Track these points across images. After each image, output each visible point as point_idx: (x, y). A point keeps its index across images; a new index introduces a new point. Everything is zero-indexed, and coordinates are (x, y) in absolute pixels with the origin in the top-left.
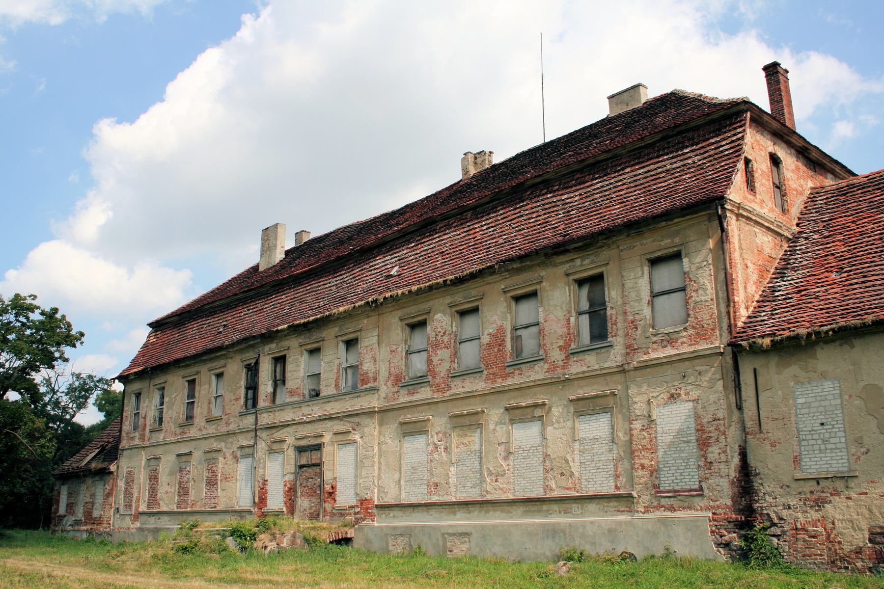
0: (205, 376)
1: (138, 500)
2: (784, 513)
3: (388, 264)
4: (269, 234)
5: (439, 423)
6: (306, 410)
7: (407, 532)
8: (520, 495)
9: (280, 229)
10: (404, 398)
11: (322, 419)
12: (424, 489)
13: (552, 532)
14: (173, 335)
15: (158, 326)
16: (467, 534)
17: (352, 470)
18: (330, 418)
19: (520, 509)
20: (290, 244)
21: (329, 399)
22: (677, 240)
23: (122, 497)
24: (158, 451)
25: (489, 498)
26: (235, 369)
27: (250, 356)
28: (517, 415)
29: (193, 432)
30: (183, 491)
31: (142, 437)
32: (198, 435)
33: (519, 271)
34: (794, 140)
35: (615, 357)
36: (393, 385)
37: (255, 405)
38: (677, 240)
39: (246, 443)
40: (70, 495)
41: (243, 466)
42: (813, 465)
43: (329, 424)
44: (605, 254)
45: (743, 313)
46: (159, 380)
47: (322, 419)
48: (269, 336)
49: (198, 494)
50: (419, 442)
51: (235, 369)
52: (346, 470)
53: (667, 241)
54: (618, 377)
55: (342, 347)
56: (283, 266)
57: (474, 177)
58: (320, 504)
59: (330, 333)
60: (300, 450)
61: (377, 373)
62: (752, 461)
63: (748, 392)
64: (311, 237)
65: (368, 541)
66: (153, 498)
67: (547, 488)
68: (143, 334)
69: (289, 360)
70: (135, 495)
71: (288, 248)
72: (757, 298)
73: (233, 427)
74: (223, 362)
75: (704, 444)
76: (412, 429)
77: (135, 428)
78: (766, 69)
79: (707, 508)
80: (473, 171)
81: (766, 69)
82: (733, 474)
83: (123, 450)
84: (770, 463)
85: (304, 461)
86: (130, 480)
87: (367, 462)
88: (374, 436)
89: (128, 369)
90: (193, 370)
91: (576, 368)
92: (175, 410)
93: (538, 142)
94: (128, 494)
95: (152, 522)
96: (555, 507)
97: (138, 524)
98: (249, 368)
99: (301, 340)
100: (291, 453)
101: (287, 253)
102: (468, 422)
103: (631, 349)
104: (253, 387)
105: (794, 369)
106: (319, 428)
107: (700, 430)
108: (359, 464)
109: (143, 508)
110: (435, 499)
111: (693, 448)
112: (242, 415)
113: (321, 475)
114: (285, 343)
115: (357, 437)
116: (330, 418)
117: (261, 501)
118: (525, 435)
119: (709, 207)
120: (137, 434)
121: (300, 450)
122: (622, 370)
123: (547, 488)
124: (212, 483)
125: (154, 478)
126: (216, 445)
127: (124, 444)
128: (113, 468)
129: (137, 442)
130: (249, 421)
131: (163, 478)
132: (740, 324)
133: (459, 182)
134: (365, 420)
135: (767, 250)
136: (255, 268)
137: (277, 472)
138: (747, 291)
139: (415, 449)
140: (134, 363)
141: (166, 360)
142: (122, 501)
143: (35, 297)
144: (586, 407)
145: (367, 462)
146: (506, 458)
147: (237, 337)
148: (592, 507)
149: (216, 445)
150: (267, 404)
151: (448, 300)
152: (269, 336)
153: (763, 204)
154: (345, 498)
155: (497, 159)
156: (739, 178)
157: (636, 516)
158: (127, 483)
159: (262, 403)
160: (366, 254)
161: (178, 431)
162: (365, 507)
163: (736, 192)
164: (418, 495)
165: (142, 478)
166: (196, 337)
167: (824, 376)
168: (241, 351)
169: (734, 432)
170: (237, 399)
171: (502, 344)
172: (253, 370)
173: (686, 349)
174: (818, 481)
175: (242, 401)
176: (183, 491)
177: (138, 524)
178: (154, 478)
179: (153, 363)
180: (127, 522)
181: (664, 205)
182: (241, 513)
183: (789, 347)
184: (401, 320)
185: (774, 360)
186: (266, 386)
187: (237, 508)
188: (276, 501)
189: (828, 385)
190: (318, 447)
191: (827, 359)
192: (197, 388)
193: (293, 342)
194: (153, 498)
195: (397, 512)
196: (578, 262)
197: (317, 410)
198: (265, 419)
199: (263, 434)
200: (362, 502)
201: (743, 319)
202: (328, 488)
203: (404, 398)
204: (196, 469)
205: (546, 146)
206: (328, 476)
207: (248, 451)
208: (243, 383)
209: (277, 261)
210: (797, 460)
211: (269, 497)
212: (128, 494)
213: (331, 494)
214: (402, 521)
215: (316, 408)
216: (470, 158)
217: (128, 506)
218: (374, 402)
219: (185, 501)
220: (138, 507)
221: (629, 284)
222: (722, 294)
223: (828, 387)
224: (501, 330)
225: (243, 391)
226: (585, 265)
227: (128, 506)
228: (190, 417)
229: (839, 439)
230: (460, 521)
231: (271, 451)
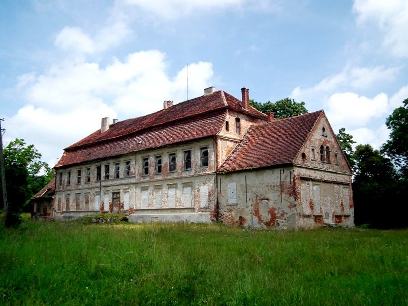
0: (84, 169)
1: (63, 208)
2: (224, 213)
3: (138, 139)
4: (104, 120)
5: (151, 188)
6: (115, 182)
7: (142, 217)
8: (170, 207)
9: (107, 119)
10: (142, 180)
11: (119, 185)
12: (147, 205)
13: (177, 217)
14: (73, 154)
15: (67, 150)
16: (157, 217)
17: (128, 200)
18: (122, 185)
19: (169, 211)
20: (111, 123)
21: (122, 179)
22: (207, 144)
23: (57, 207)
24: (69, 192)
25: (163, 208)
26: (93, 168)
27: (98, 164)
28: (170, 186)
29: (80, 187)
30: (78, 205)
31: (63, 188)
32: (82, 187)
33: (171, 147)
34: (245, 113)
35: (192, 173)
36: (139, 176)
37: (100, 179)
38: (207, 144)
39: (97, 191)
40: (38, 206)
41: (97, 197)
42: (230, 202)
43: (122, 186)
44: (192, 145)
45: (220, 164)
46: (68, 170)
47: (119, 185)
48: (104, 159)
49: (83, 206)
50: (146, 193)
51: (93, 168)
52: (127, 200)
53: (204, 144)
54: (193, 178)
55: (125, 163)
56: (109, 132)
57: (167, 109)
58: (120, 209)
59: (122, 159)
60: (114, 193)
61: (135, 172)
62: (219, 201)
63: (219, 184)
64: (119, 121)
65: (132, 219)
66: (68, 207)
67: (176, 206)
68: (61, 154)
69: (110, 167)
70: (62, 206)
71: (110, 124)
72: (225, 159)
73: (93, 186)
74: (90, 165)
75: (210, 196)
76: (144, 189)
77: (61, 184)
78: (242, 89)
79: (209, 212)
80: (167, 107)
81: (242, 89)
82: (215, 203)
83: (57, 192)
84: (223, 202)
85: (115, 197)
86: (59, 201)
87: (132, 198)
88: (135, 191)
89: (57, 165)
90: (80, 167)
91: (184, 175)
92: (74, 179)
93: (186, 100)
94: (59, 206)
95: (68, 215)
96: (178, 211)
97: (63, 215)
98: (98, 168)
99: (113, 161)
100: (111, 194)
101: (111, 126)
102: (158, 188)
103: (196, 171)
104: (99, 174)
105: (228, 179)
106: (119, 187)
107: (209, 193)
108: (130, 198)
109: (64, 210)
110: (150, 208)
111: (207, 197)
112: (96, 182)
113: (120, 201)
114: (109, 161)
115: (129, 190)
116: (122, 185)
117: (103, 208)
118: (172, 192)
119: (214, 138)
120: (61, 187)
121: (114, 193)
122: (193, 176)
123: (176, 206)
124: (87, 203)
125: (68, 201)
126: (88, 191)
127: (57, 190)
128: (53, 197)
129: (61, 189)
130: (99, 184)
131: (71, 201)
132: (219, 167)
133: (162, 110)
134: (132, 186)
135: (231, 146)
136: (99, 132)
137: (107, 200)
138: (222, 157)
139: (145, 195)
140: (59, 163)
141: (71, 163)
142: (57, 208)
143: (23, 140)
144: (185, 185)
145: (132, 198)
146: (167, 198)
147: (94, 158)
148: (186, 211)
149: (88, 191)
150: (104, 179)
151: (154, 153)
152: (104, 159)
153: (232, 134)
154: (126, 208)
155: (175, 104)
156: (224, 127)
157: (195, 213)
158: (58, 202)
159: (102, 179)
160: (132, 135)
161: (76, 186)
162: (132, 210)
163: (222, 133)
164: (145, 207)
165: (64, 201)
166: (80, 156)
167: (233, 181)
168: (95, 162)
169: (216, 193)
170: (94, 177)
171: (167, 167)
172: (99, 169)
173: (207, 172)
174: (231, 206)
175: (96, 178)
176: (78, 205)
177: (63, 215)
178: (68, 201)
179: (66, 164)
180: (59, 215)
181: (204, 134)
182: (96, 212)
183: (229, 173)
184: (142, 157)
185: (224, 176)
186: (103, 174)
187: (95, 210)
188: (107, 208)
189: (234, 184)
190: (119, 193)
191: (235, 177)
192: (82, 173)
193: (111, 161)
194: (68, 207)
195: (140, 212)
196: (185, 147)
197: (118, 182)
198: (103, 184)
199: (103, 188)
200: (131, 209)
201: (220, 166)
202: (121, 205)
203: (142, 180)
204: (82, 199)
205: (188, 102)
206: (121, 201)
207: (99, 193)
208: (96, 172)
209: (107, 130)
210: (227, 201)
211: (105, 207)
212: (59, 206)
213: (122, 207)
214: (141, 214)
215: (118, 182)
216: (166, 102)
217: (59, 210)
218: (133, 181)
219: (79, 208)
220: (63, 210)
221: (196, 154)
222: (215, 159)
223: (234, 184)
224: (166, 163)
225: (96, 175)
226: (187, 148)
227: (59, 210)
228: (79, 182)
229: (235, 196)
230: (156, 214)
231: (105, 194)
